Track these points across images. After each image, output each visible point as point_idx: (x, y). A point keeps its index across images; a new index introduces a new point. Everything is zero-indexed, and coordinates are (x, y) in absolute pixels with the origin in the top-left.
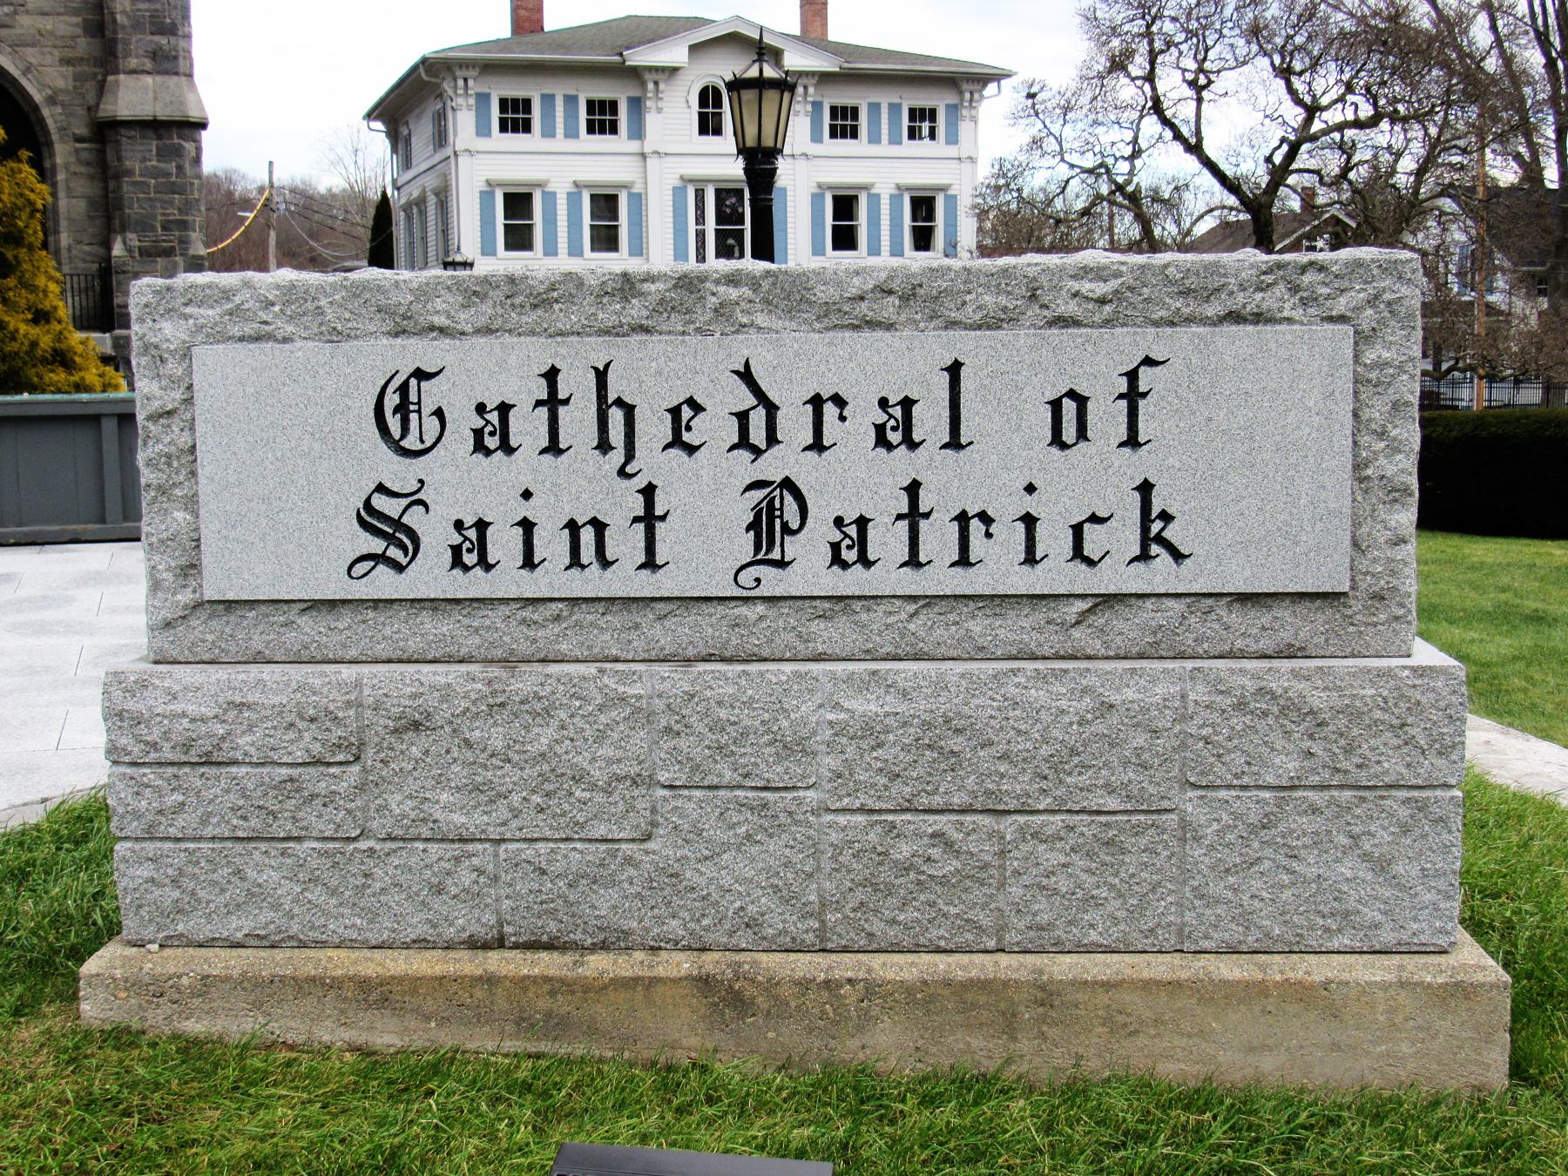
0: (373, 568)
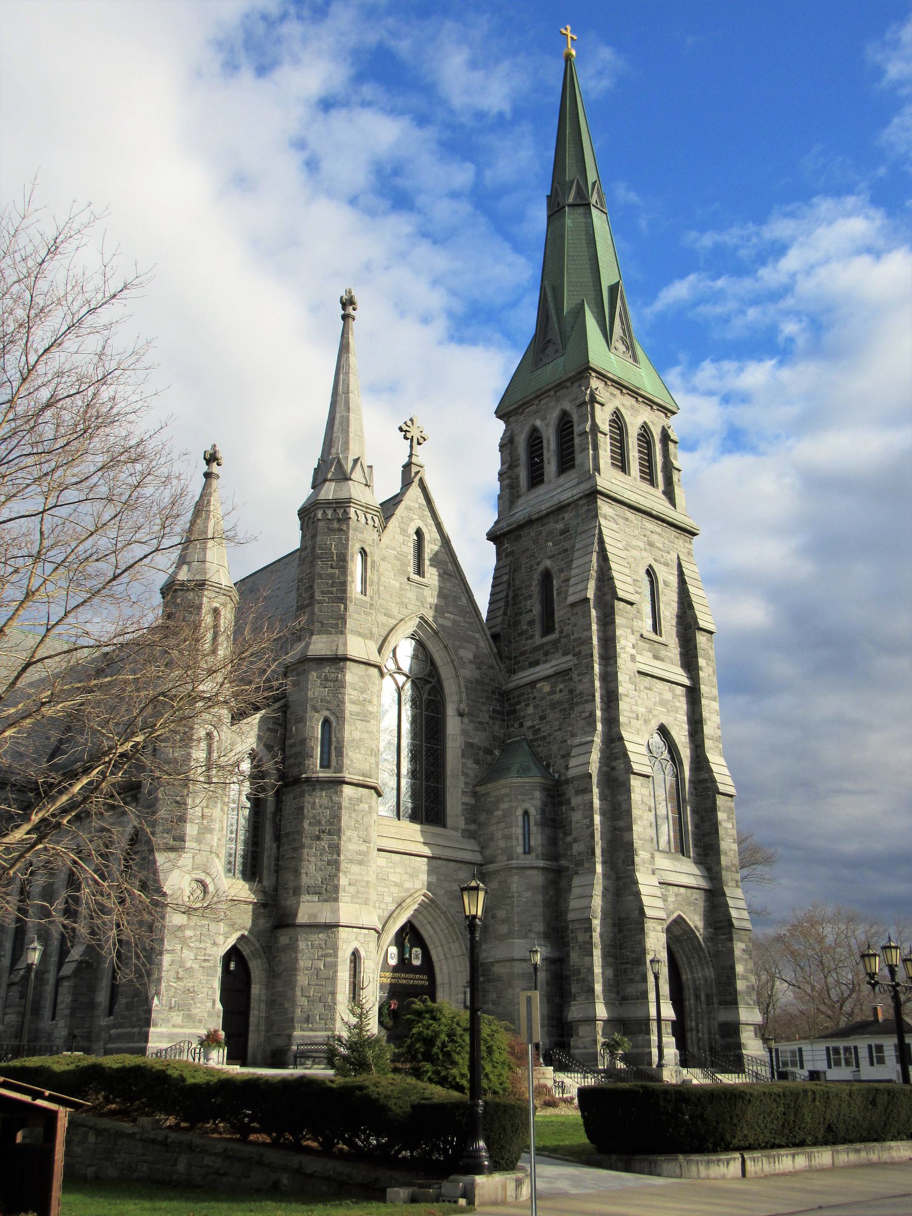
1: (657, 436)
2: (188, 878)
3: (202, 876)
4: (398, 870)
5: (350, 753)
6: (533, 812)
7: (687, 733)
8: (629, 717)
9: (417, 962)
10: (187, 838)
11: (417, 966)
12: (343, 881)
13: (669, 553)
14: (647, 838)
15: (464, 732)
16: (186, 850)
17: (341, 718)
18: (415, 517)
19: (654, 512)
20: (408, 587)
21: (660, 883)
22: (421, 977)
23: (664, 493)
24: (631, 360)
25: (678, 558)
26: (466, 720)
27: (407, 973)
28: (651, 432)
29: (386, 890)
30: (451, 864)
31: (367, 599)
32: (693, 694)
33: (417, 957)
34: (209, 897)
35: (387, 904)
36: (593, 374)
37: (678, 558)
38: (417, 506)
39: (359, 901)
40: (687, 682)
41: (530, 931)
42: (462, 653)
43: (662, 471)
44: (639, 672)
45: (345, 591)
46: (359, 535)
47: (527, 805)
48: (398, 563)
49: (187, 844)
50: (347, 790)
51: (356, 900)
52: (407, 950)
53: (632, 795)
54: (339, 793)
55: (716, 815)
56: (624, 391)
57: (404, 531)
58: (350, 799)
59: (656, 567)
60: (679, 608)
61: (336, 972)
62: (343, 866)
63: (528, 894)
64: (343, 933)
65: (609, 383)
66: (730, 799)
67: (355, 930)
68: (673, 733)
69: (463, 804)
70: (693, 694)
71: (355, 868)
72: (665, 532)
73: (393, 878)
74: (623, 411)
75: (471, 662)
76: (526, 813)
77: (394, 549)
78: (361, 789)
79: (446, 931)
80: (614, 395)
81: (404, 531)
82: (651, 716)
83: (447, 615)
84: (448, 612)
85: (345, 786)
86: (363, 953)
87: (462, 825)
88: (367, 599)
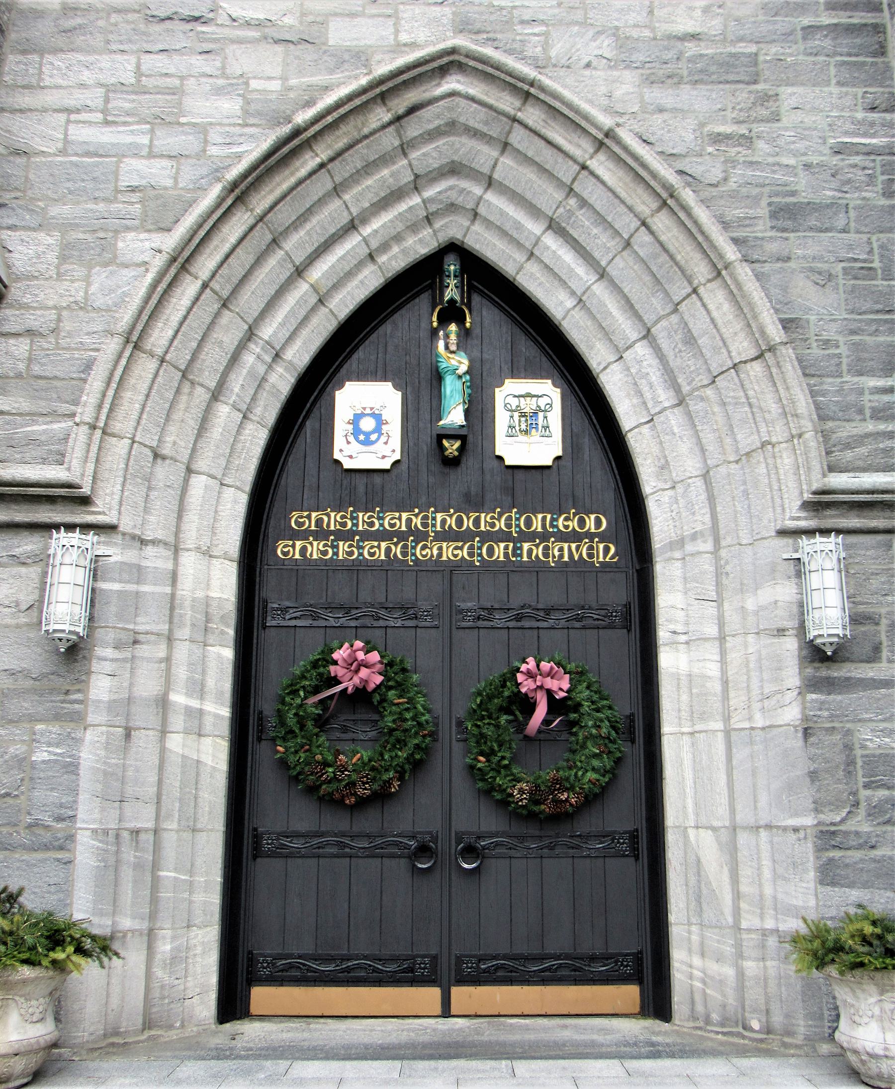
22: (566, 523)
29: (199, 63)
35: (202, 130)
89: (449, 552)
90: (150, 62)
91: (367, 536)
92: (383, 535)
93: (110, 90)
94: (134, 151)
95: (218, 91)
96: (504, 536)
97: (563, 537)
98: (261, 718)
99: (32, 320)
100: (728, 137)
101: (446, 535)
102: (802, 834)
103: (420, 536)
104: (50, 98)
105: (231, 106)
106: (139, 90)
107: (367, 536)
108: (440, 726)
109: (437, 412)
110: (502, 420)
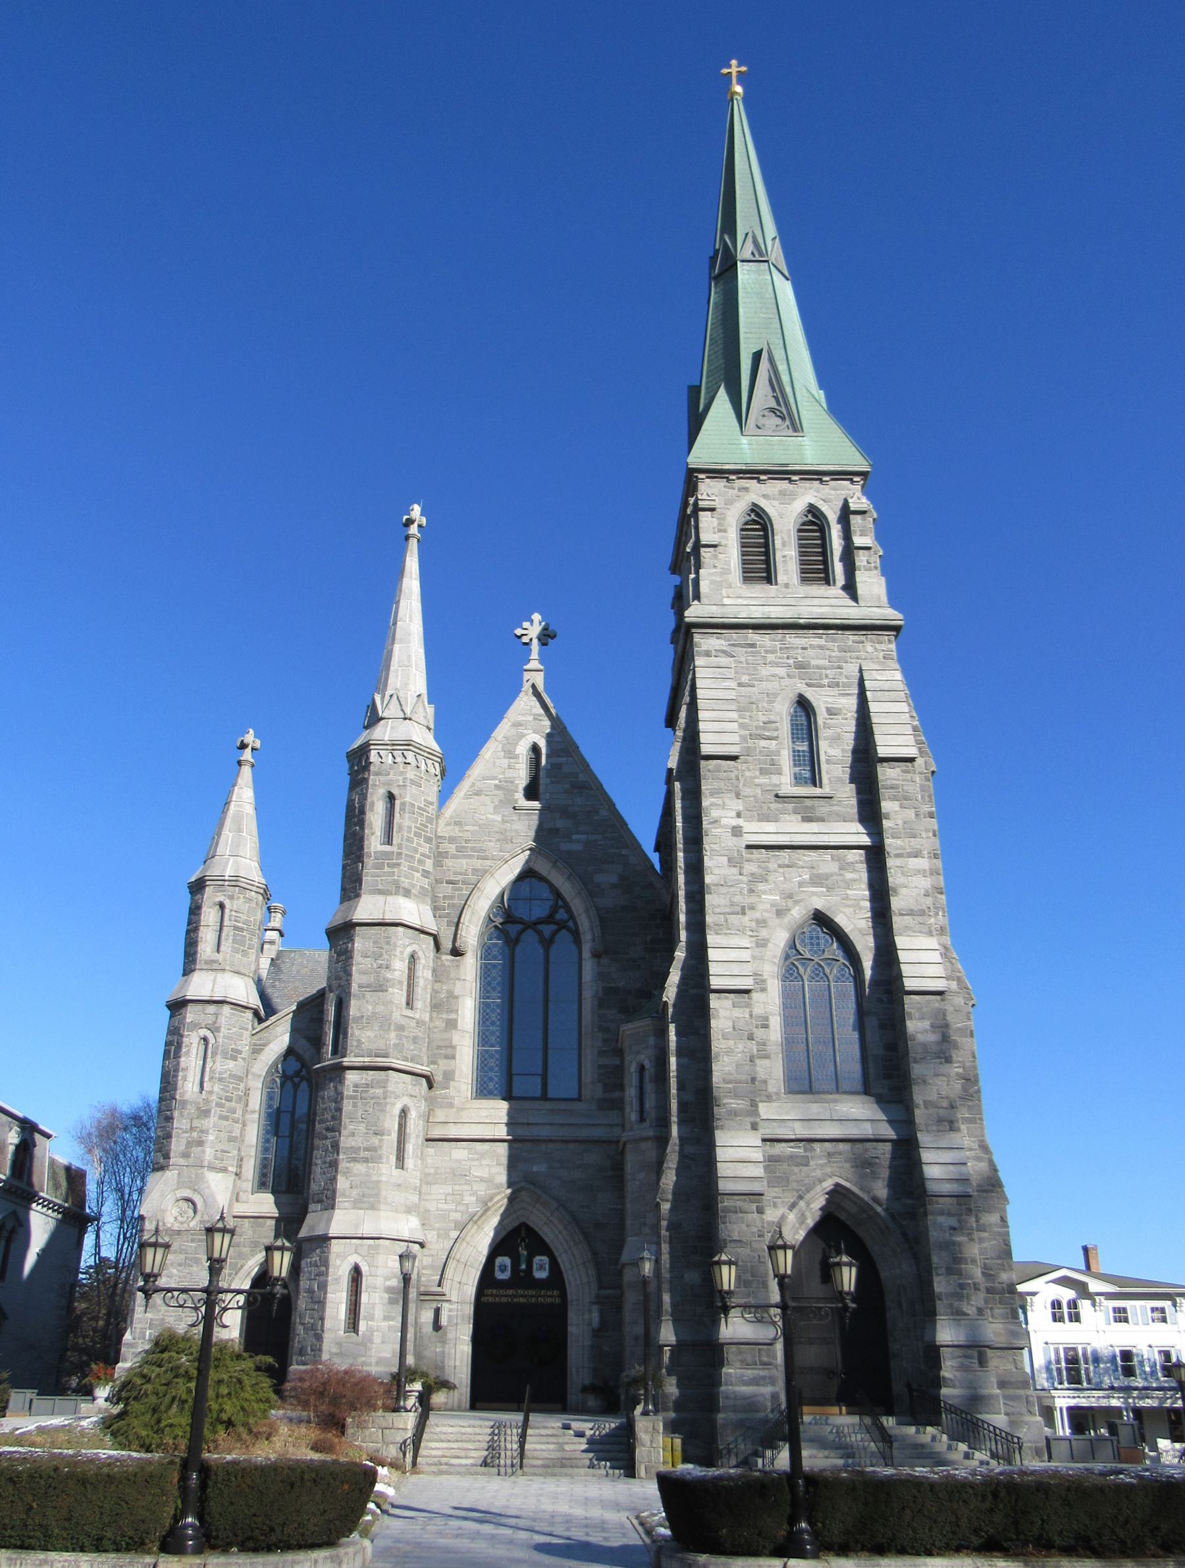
0: (214, 981)
1: (832, 515)
2: (171, 1198)
3: (187, 1193)
4: (485, 1162)
5: (357, 1032)
6: (647, 1064)
7: (869, 914)
8: (724, 914)
9: (541, 1275)
10: (172, 1155)
11: (541, 1280)
12: (342, 1183)
13: (840, 667)
14: (743, 1077)
15: (601, 976)
16: (171, 1168)
17: (349, 994)
18: (525, 731)
19: (802, 621)
20: (515, 818)
21: (764, 1140)
22: (549, 1293)
23: (844, 588)
24: (791, 432)
25: (861, 671)
26: (604, 961)
27: (529, 1288)
28: (822, 513)
29: (467, 1188)
30: (572, 1146)
31: (394, 849)
32: (876, 857)
33: (541, 1268)
34: (199, 1213)
35: (467, 1205)
36: (700, 476)
37: (861, 671)
38: (531, 718)
39: (364, 1206)
40: (866, 840)
41: (645, 1224)
42: (599, 878)
43: (841, 560)
44: (749, 847)
45: (361, 848)
46: (382, 778)
47: (642, 1057)
48: (500, 792)
49: (172, 1161)
50: (351, 1077)
51: (360, 1205)
52: (523, 1259)
53: (713, 1023)
54: (341, 1080)
55: (905, 1026)
56: (763, 477)
57: (510, 754)
58: (356, 1086)
59: (810, 694)
60: (856, 739)
61: (326, 1293)
62: (343, 1165)
63: (641, 1176)
64: (336, 1247)
65: (733, 477)
66: (938, 997)
67: (353, 1241)
68: (841, 920)
69: (600, 1067)
70: (876, 857)
71: (359, 1168)
72: (834, 641)
73: (477, 1173)
74: (763, 503)
75: (614, 886)
76: (642, 1069)
77: (494, 778)
78: (371, 1072)
79: (564, 1232)
80: (746, 489)
81: (510, 754)
82: (790, 903)
83: (574, 837)
84: (578, 834)
85: (348, 1072)
86: (364, 1269)
87: (599, 1092)
88: (394, 849)
89: (522, 1300)
90: (457, 1187)
91: (503, 1296)
92: (506, 1296)
93: (447, 1195)
94: (451, 1210)
95: (471, 1195)
96: (533, 1296)
97: (550, 1296)
98: (245, 1012)
99: (432, 1252)
100: (910, 855)
101: (521, 1296)
102: (316, 1199)
103: (515, 1296)
104: (434, 1197)
105: (473, 1199)
106: (453, 1194)
107: (503, 1296)
108: (273, 1019)
109: (519, 1265)
110: (535, 1266)
